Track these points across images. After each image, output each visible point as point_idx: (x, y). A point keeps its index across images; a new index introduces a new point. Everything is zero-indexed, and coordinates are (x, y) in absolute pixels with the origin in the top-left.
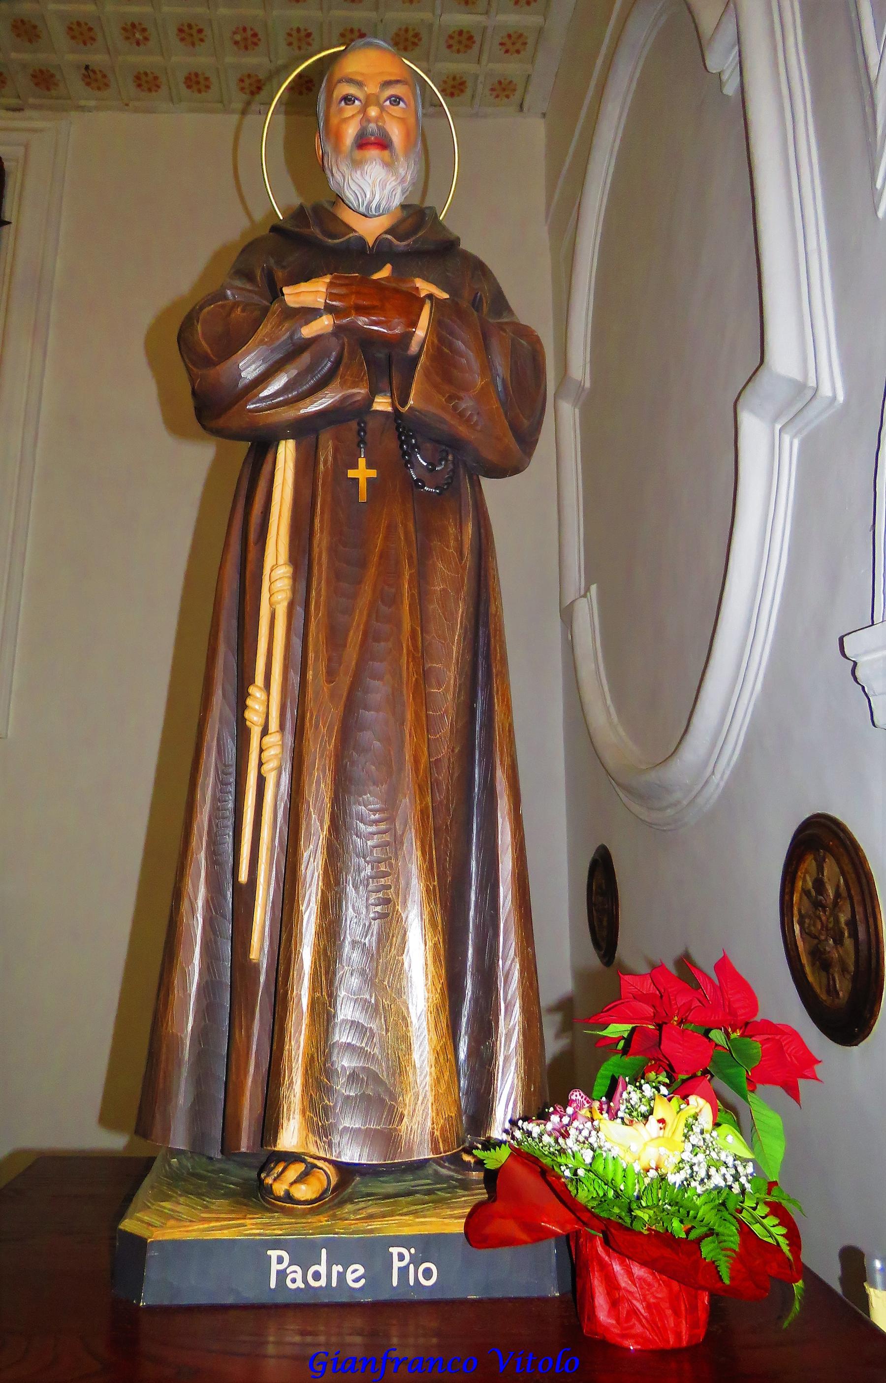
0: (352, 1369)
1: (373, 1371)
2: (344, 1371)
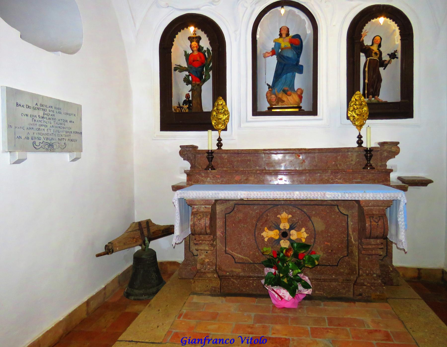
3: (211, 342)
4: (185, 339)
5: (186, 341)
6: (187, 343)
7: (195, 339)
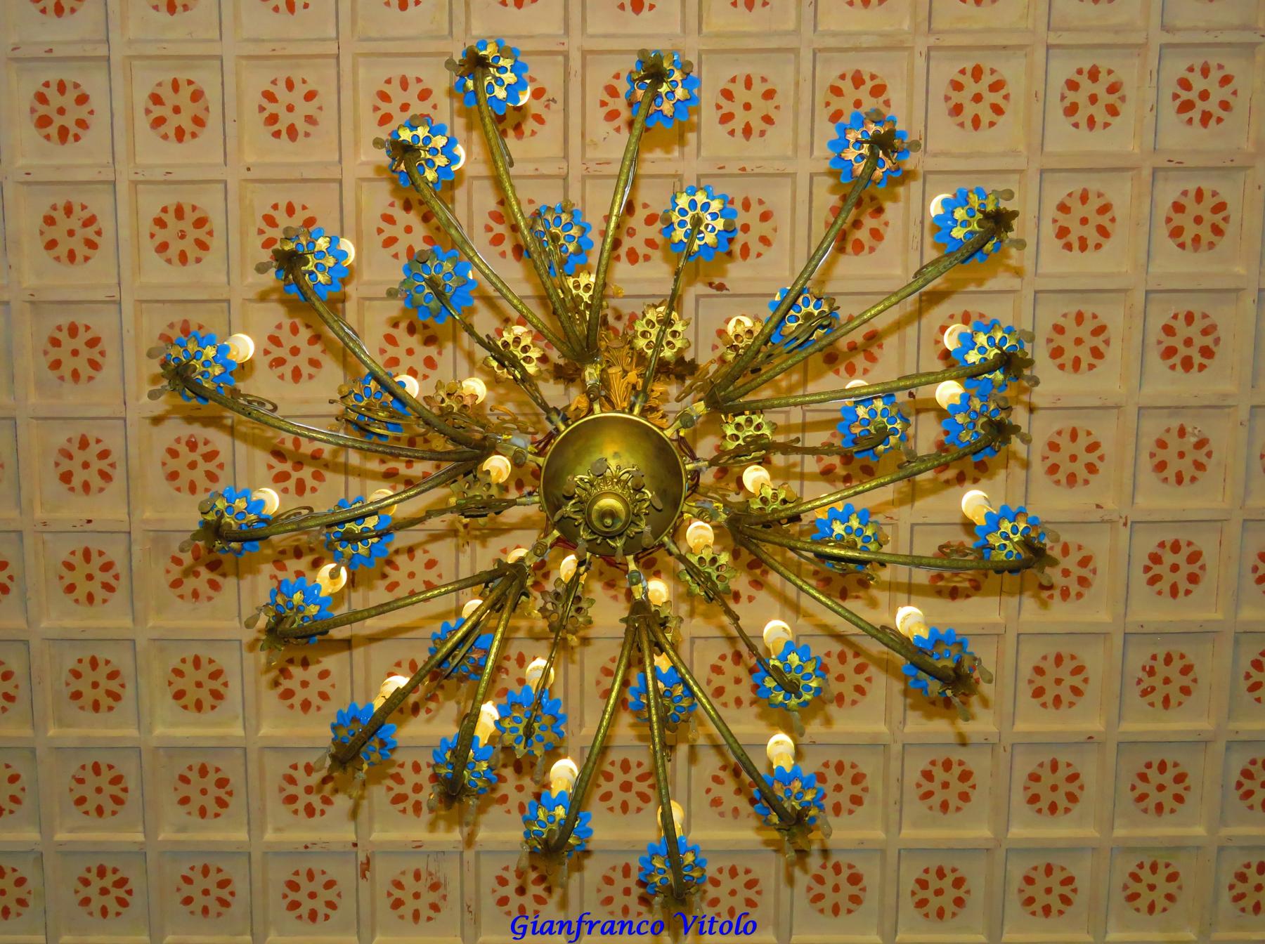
0: (550, 931)
1: (569, 933)
2: (543, 933)
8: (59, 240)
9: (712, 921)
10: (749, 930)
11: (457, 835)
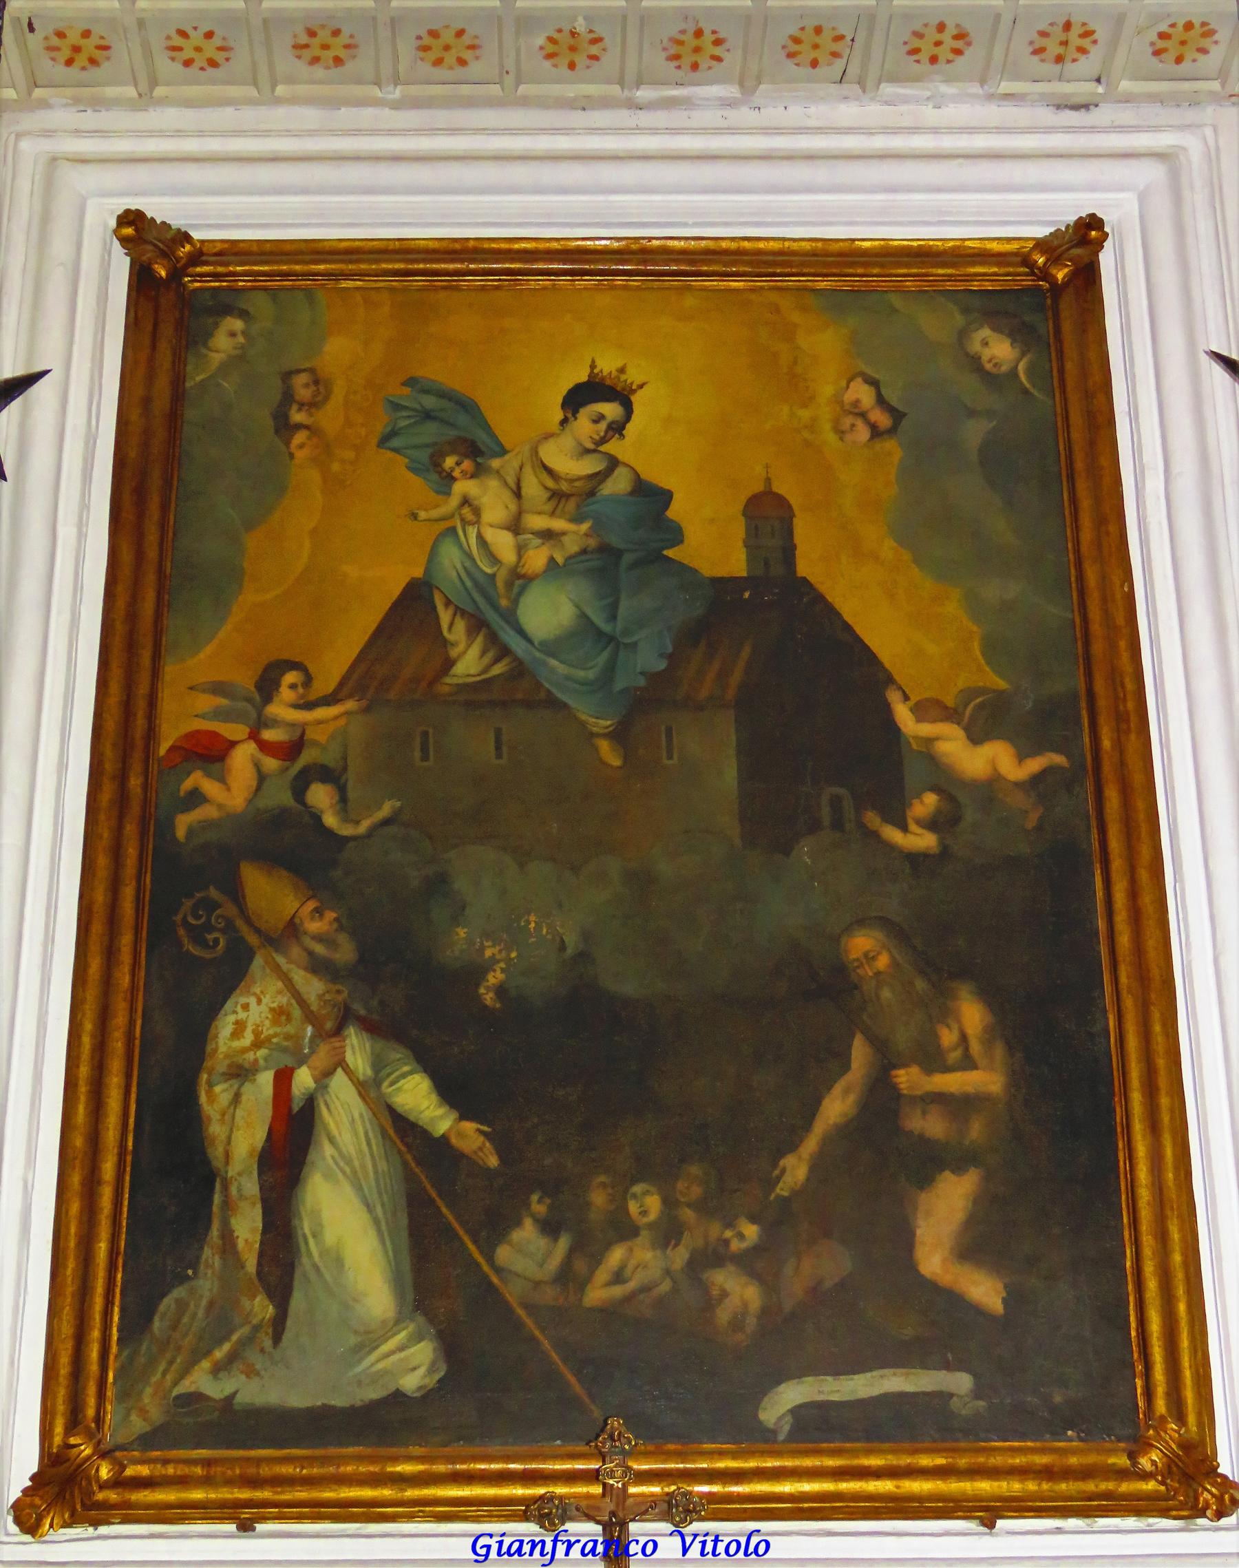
3: (576, 1551)
4: (483, 1541)
5: (489, 1547)
6: (493, 1554)
7: (521, 1542)
8: (926, 38)
9: (716, 1541)
10: (761, 1551)
11: (731, 694)
